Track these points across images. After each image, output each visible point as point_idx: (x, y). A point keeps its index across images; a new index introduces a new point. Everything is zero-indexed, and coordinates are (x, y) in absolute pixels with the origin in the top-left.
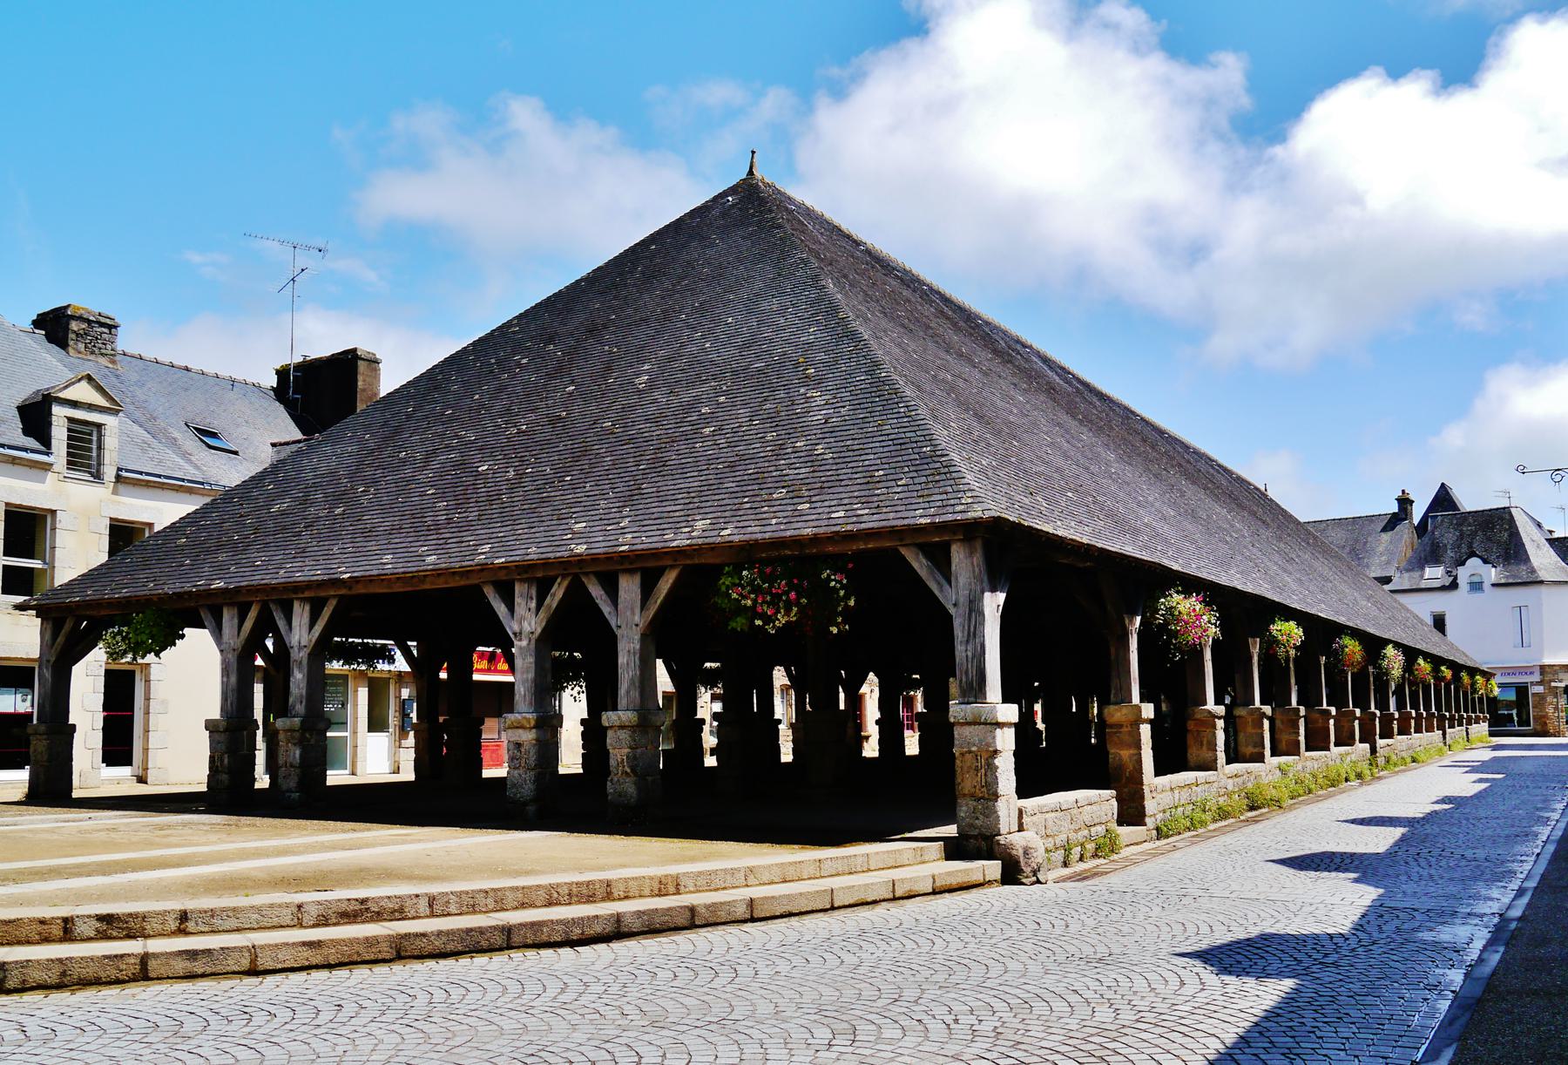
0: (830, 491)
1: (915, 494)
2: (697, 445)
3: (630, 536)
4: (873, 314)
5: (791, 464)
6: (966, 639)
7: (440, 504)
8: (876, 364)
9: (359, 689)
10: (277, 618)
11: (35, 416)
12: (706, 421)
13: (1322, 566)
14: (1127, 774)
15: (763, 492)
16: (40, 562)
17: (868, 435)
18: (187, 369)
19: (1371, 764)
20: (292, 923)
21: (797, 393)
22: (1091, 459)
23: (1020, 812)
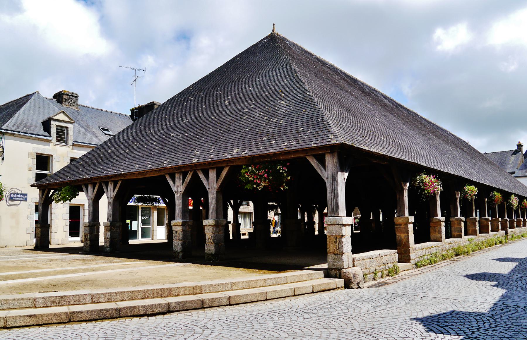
0: (283, 136)
1: (313, 136)
2: (241, 123)
3: (212, 155)
4: (311, 75)
5: (271, 127)
6: (331, 191)
7: (157, 147)
8: (306, 90)
9: (154, 212)
10: (104, 188)
11: (46, 125)
12: (245, 114)
13: (488, 167)
14: (404, 243)
15: (259, 138)
16: (49, 172)
17: (299, 115)
18: (102, 110)
19: (505, 238)
20: (32, 306)
21: (277, 103)
22: (396, 128)
23: (354, 259)
